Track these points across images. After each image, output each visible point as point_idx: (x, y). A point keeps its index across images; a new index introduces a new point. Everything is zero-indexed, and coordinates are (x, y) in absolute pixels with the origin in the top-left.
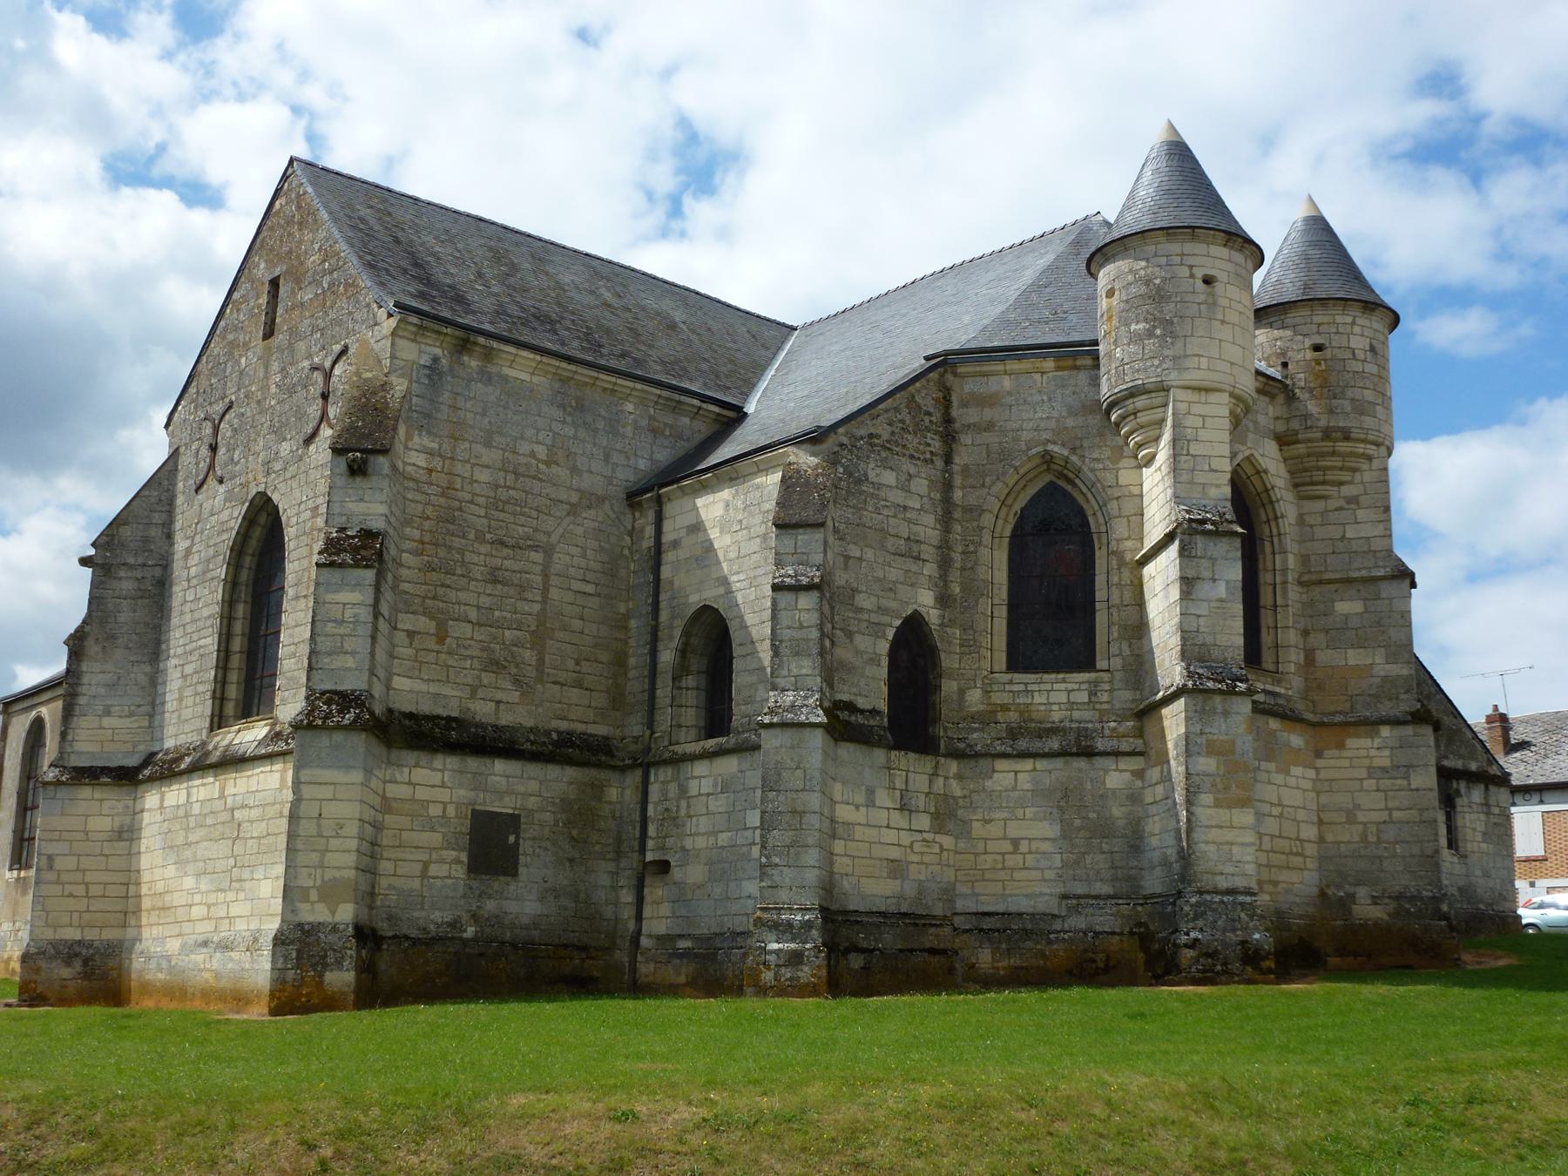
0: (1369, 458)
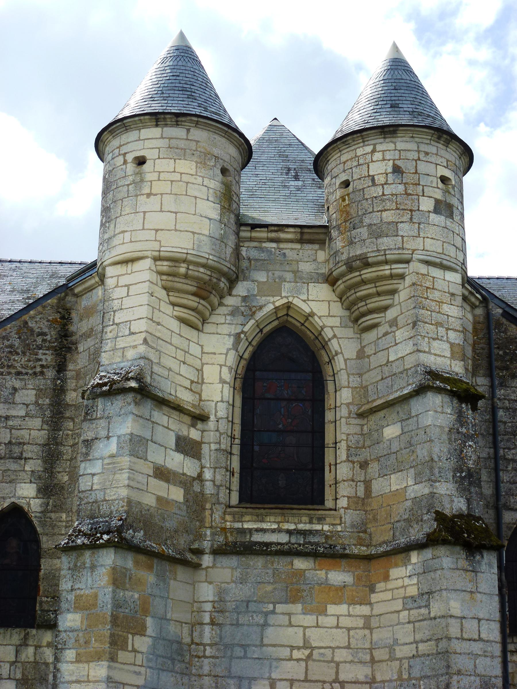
0: (402, 277)
